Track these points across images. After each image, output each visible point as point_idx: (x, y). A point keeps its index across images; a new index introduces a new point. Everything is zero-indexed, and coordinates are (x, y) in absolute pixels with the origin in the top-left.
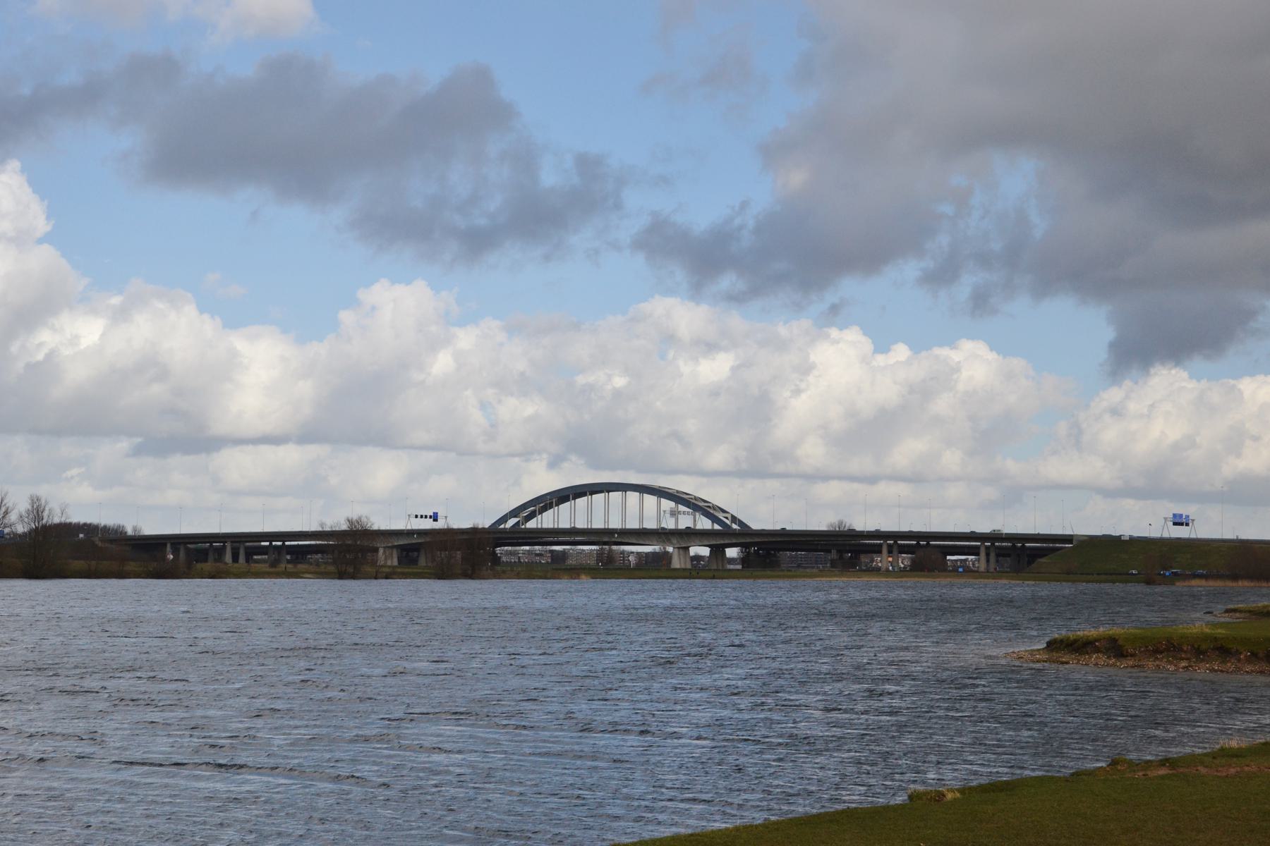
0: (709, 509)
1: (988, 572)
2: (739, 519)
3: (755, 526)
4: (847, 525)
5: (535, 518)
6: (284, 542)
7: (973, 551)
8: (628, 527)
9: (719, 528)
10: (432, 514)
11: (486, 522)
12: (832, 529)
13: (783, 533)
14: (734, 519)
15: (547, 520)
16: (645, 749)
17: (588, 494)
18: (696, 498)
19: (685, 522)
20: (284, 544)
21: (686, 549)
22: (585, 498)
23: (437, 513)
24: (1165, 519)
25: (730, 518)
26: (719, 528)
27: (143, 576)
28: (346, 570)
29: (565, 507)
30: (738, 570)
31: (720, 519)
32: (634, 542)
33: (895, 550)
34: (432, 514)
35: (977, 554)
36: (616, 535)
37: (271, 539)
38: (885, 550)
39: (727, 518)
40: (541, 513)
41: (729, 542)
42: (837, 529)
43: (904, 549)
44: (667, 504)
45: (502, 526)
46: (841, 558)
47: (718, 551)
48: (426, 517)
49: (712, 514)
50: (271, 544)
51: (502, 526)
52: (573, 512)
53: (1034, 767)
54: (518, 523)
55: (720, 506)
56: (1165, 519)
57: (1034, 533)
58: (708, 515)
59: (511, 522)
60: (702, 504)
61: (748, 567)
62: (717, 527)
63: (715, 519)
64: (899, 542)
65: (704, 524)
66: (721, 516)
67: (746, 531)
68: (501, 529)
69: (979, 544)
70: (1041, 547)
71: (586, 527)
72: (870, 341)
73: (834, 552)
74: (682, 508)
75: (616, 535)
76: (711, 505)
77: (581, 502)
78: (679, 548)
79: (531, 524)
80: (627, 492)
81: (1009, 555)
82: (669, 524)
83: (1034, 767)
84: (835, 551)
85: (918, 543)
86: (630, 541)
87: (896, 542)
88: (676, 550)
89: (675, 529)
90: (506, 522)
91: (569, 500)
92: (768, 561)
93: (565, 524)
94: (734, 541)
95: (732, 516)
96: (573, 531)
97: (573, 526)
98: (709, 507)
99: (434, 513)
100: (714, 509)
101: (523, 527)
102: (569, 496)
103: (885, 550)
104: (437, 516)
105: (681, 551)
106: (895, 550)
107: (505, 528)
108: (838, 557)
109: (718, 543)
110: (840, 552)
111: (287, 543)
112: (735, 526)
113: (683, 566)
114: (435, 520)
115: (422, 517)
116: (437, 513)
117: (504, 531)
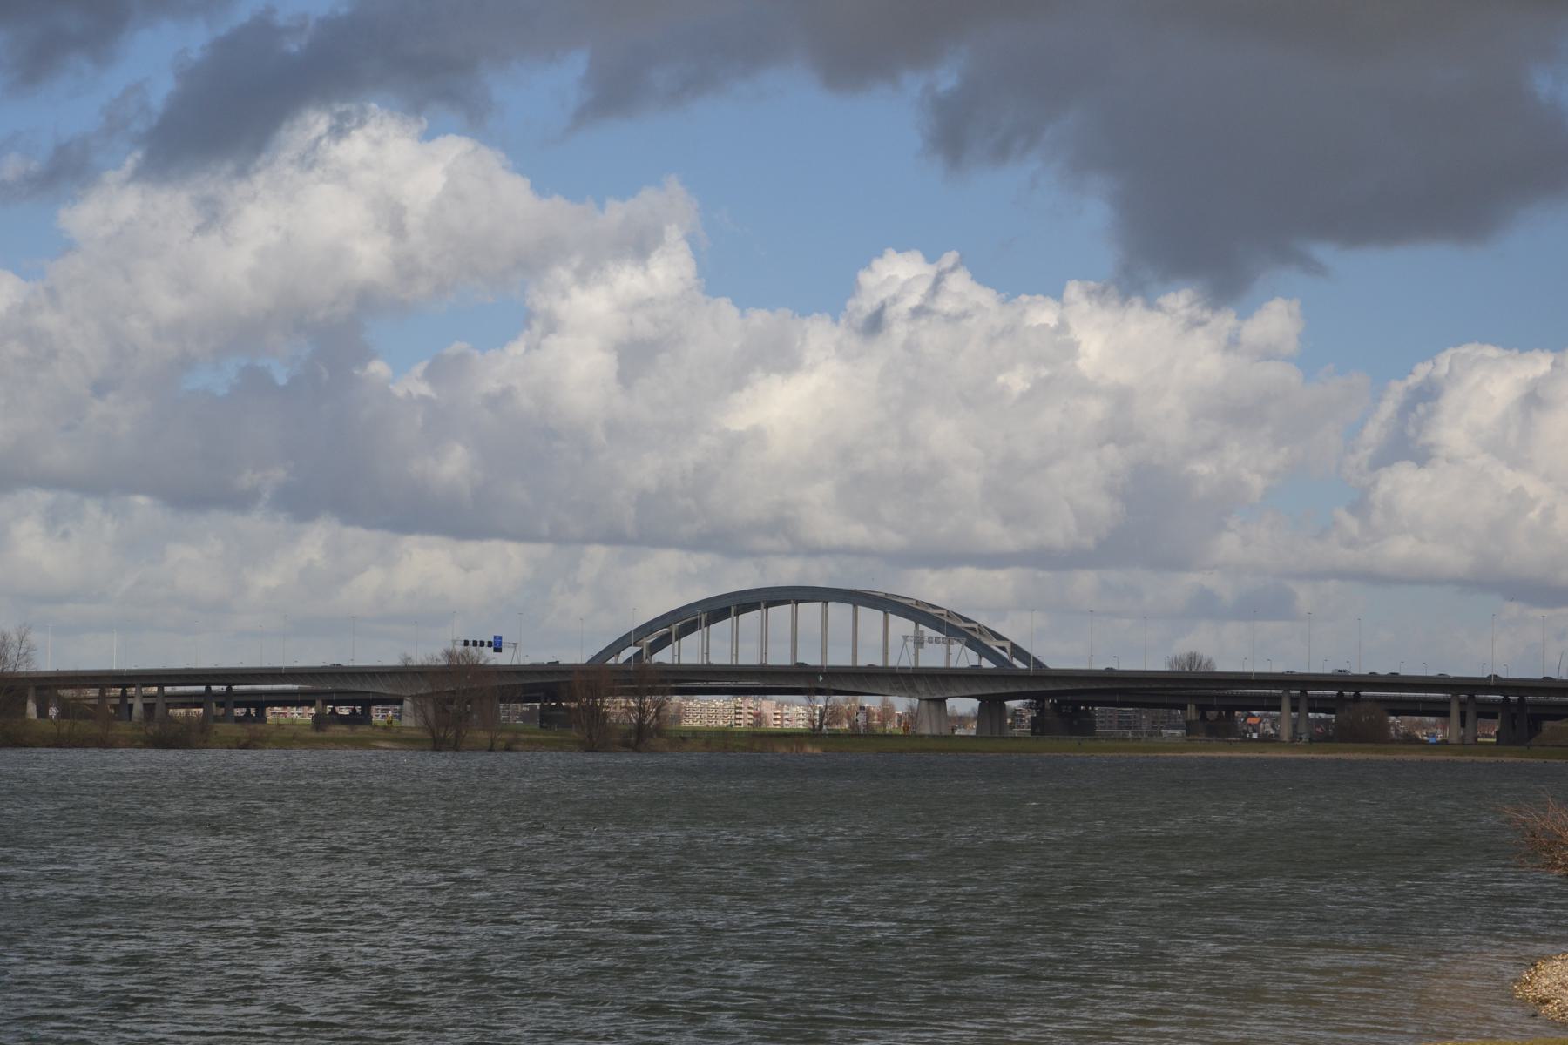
0: (973, 634)
1: (1463, 744)
2: (1034, 658)
3: (1053, 663)
4: (1204, 662)
5: (671, 646)
6: (230, 686)
7: (1440, 710)
8: (741, 662)
9: (992, 666)
10: (492, 640)
11: (576, 655)
12: (1176, 668)
13: (1110, 676)
14: (1018, 652)
15: (689, 651)
16: (120, 968)
17: (763, 605)
18: (949, 614)
19: (935, 655)
20: (229, 689)
21: (941, 702)
22: (757, 613)
23: (500, 638)
24: (905, 638)
25: (1009, 649)
26: (992, 666)
27: (139, 743)
28: (445, 736)
29: (722, 627)
30: (1492, 743)
31: (993, 650)
32: (852, 689)
33: (1303, 705)
34: (492, 640)
35: (1446, 714)
36: (821, 678)
37: (208, 681)
38: (1286, 704)
39: (1003, 649)
40: (679, 638)
41: (1018, 690)
42: (1187, 669)
43: (1486, 711)
44: (902, 627)
45: (611, 661)
46: (1203, 717)
47: (992, 706)
48: (482, 644)
49: (979, 642)
50: (208, 689)
51: (611, 661)
52: (735, 638)
53: (654, 986)
54: (639, 655)
55: (985, 625)
56: (905, 638)
57: (1480, 676)
58: (973, 644)
59: (628, 653)
60: (962, 625)
61: (1042, 734)
62: (987, 664)
63: (984, 651)
64: (1309, 692)
65: (964, 658)
66: (994, 644)
67: (1040, 674)
68: (610, 665)
69: (1281, 691)
70: (1444, 698)
71: (700, 662)
72: (816, 315)
73: (1191, 708)
74: (928, 632)
75: (821, 678)
76: (976, 626)
77: (750, 619)
78: (928, 700)
79: (664, 656)
80: (829, 604)
81: (1494, 716)
82: (901, 658)
83: (654, 986)
84: (1194, 707)
85: (1340, 695)
86: (843, 689)
87: (1304, 692)
88: (924, 703)
89: (883, 668)
90: (619, 653)
91: (728, 616)
92: (1075, 723)
93: (749, 656)
94: (1025, 689)
95: (1013, 646)
96: (763, 671)
97: (764, 662)
98: (973, 629)
99: (495, 637)
100: (981, 633)
101: (647, 661)
102: (729, 609)
103: (1286, 704)
104: (500, 643)
105: (933, 706)
106: (1303, 705)
107: (616, 665)
108: (1198, 717)
109: (998, 692)
110: (1202, 708)
111: (202, 688)
112: (1020, 665)
113: (935, 732)
114: (498, 650)
115: (475, 643)
116: (500, 638)
117: (616, 670)
